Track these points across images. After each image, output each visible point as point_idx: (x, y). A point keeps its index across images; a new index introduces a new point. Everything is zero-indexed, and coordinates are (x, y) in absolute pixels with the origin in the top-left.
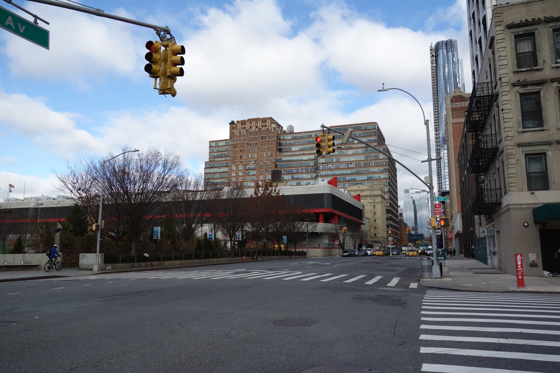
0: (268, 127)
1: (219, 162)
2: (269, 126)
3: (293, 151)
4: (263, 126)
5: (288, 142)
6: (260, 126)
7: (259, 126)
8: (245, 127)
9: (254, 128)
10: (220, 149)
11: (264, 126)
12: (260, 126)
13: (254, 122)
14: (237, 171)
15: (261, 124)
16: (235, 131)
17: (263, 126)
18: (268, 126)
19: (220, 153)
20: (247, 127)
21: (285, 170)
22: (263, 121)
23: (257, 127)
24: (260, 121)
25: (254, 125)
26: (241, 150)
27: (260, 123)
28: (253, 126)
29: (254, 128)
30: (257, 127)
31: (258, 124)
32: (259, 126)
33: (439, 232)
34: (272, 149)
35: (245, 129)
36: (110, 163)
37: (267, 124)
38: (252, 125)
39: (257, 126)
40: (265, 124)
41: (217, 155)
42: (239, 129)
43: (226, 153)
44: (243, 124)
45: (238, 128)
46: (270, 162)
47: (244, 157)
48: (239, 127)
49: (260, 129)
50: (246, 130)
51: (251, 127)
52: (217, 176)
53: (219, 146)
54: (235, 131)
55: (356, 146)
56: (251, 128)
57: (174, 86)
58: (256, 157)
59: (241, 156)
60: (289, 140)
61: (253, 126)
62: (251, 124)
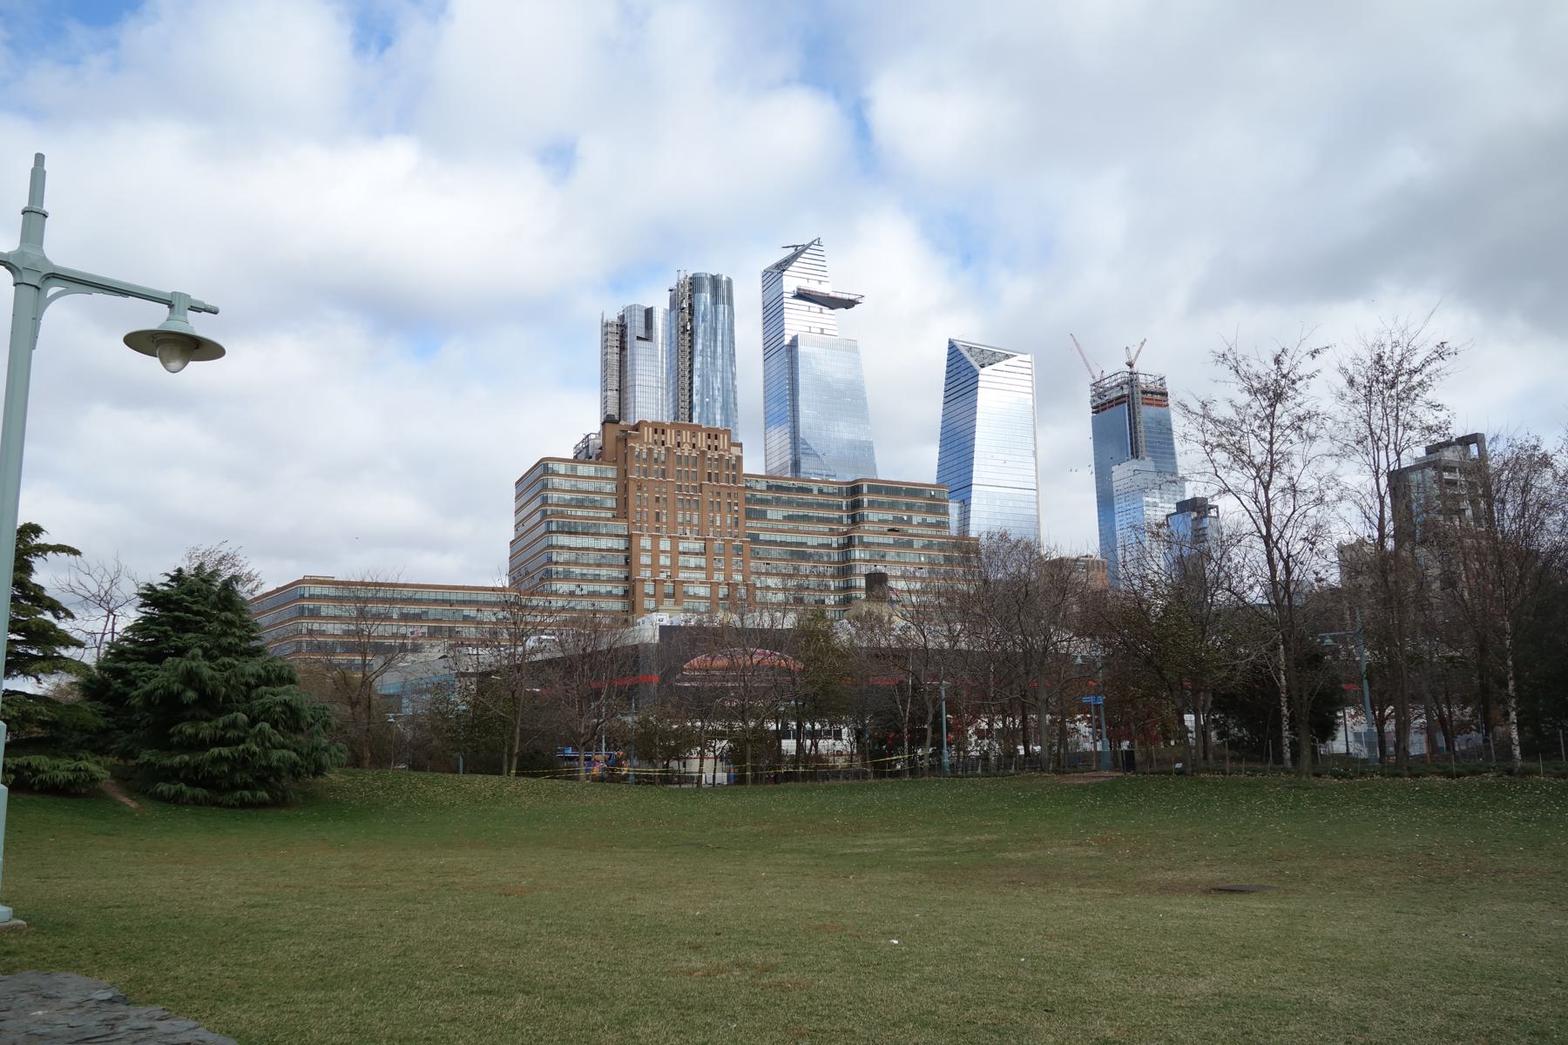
0: (722, 453)
1: (595, 520)
3: (770, 520)
4: (709, 447)
5: (759, 495)
6: (702, 444)
7: (699, 445)
8: (663, 442)
9: (686, 448)
10: (583, 485)
11: (713, 447)
12: (702, 444)
13: (688, 433)
14: (655, 553)
15: (706, 442)
16: (638, 445)
17: (709, 446)
18: (725, 451)
19: (580, 496)
20: (669, 442)
21: (768, 564)
22: (709, 435)
23: (694, 446)
24: (704, 434)
25: (688, 441)
26: (657, 499)
28: (684, 441)
29: (686, 448)
30: (694, 447)
31: (697, 440)
32: (699, 445)
33: (802, 295)
34: (736, 508)
35: (663, 444)
36: (1254, 466)
37: (719, 443)
38: (682, 439)
39: (694, 445)
40: (716, 443)
41: (572, 499)
42: (648, 443)
43: (597, 497)
44: (659, 431)
45: (646, 440)
46: (740, 541)
47: (664, 517)
48: (702, 437)
49: (704, 453)
50: (668, 449)
51: (679, 443)
52: (592, 557)
53: (576, 476)
54: (638, 445)
55: (915, 532)
56: (679, 446)
57: (55, 264)
58: (695, 521)
59: (658, 514)
60: (761, 491)
62: (694, 437)
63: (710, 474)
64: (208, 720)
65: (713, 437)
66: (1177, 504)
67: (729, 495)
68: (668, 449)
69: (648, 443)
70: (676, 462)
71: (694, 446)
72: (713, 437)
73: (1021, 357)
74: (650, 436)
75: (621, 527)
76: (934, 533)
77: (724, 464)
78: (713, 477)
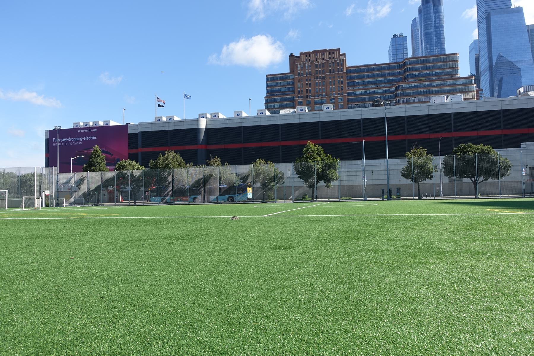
2: (338, 58)
7: (326, 58)
9: (320, 61)
11: (332, 58)
23: (323, 59)
25: (321, 57)
27: (328, 55)
28: (319, 58)
29: (320, 61)
40: (333, 55)
49: (328, 61)
50: (311, 62)
56: (316, 60)
61: (319, 58)
69: (303, 62)
74: (304, 58)
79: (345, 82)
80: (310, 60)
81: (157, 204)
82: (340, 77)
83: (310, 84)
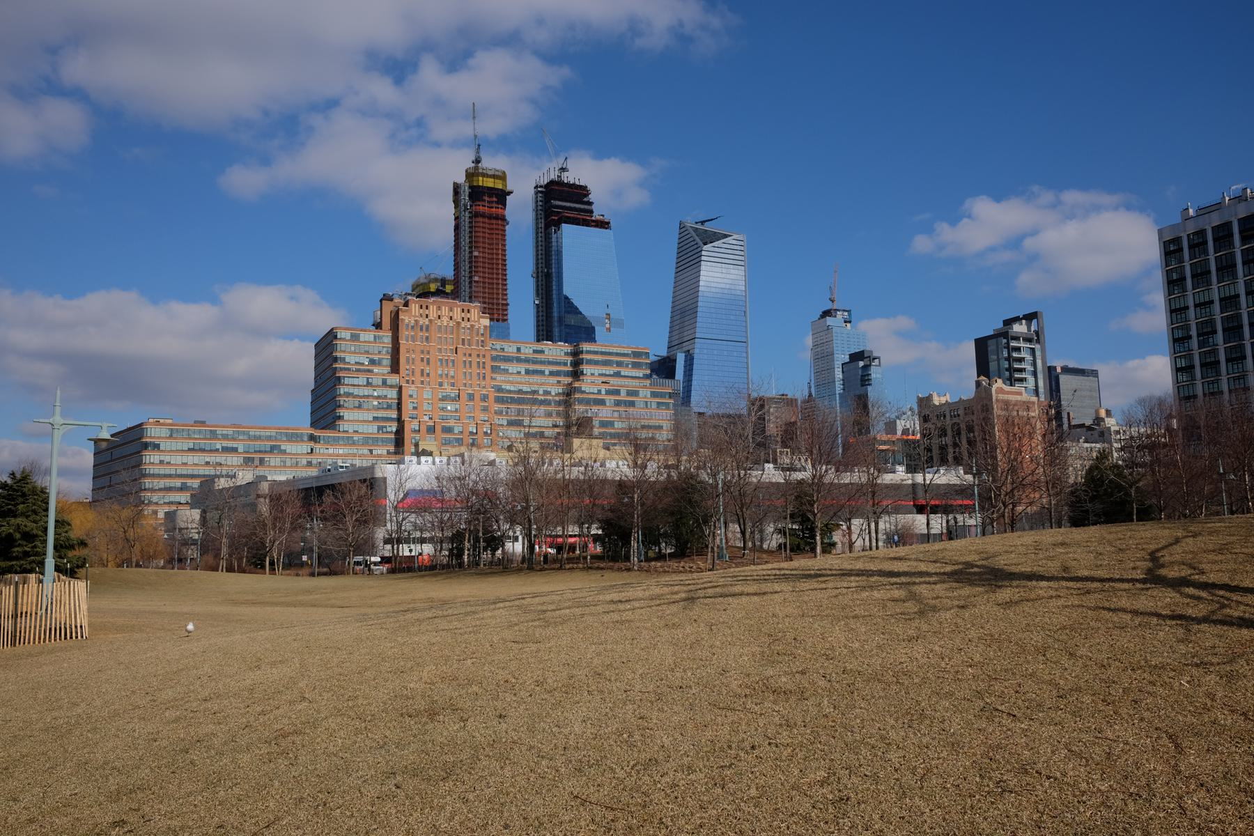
4: (463, 319)
9: (445, 320)
11: (466, 319)
23: (451, 318)
29: (445, 320)
40: (468, 315)
49: (458, 323)
50: (431, 321)
56: (439, 318)
63: (463, 340)
64: (592, 428)
65: (466, 311)
66: (850, 355)
67: (478, 356)
68: (431, 321)
69: (415, 316)
70: (437, 330)
71: (451, 318)
72: (466, 311)
73: (735, 236)
75: (393, 379)
76: (638, 384)
77: (475, 332)
78: (466, 342)
79: (488, 367)
80: (427, 316)
81: (1054, 388)
82: (425, 352)
83: (484, 363)
